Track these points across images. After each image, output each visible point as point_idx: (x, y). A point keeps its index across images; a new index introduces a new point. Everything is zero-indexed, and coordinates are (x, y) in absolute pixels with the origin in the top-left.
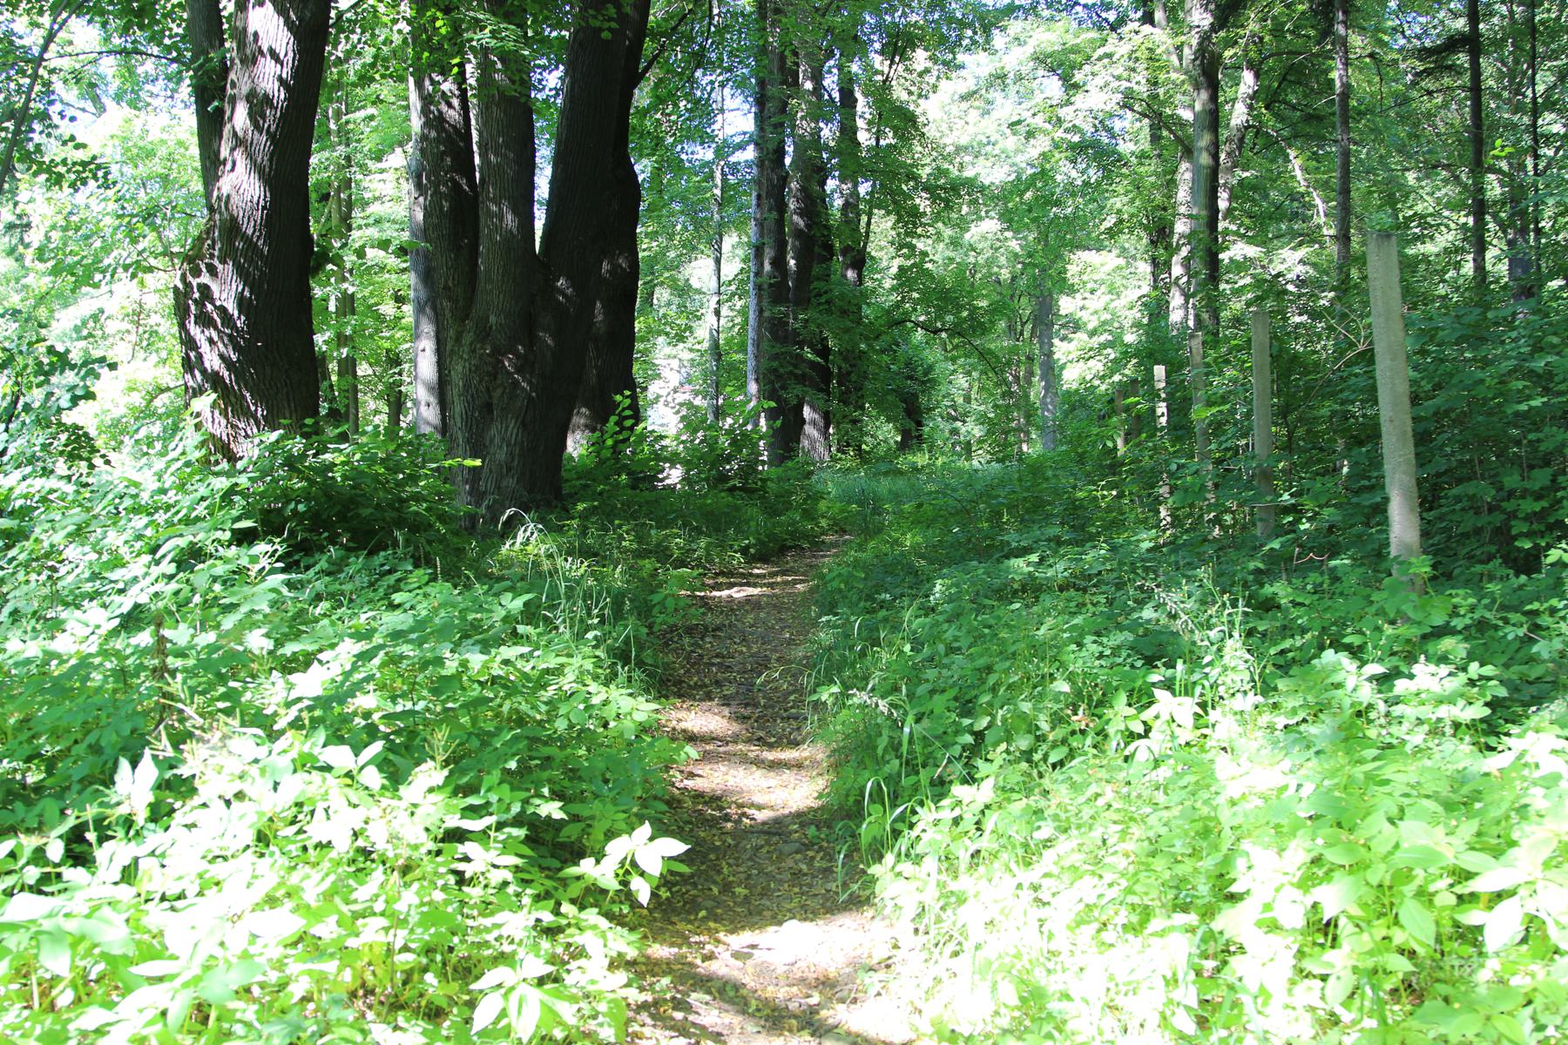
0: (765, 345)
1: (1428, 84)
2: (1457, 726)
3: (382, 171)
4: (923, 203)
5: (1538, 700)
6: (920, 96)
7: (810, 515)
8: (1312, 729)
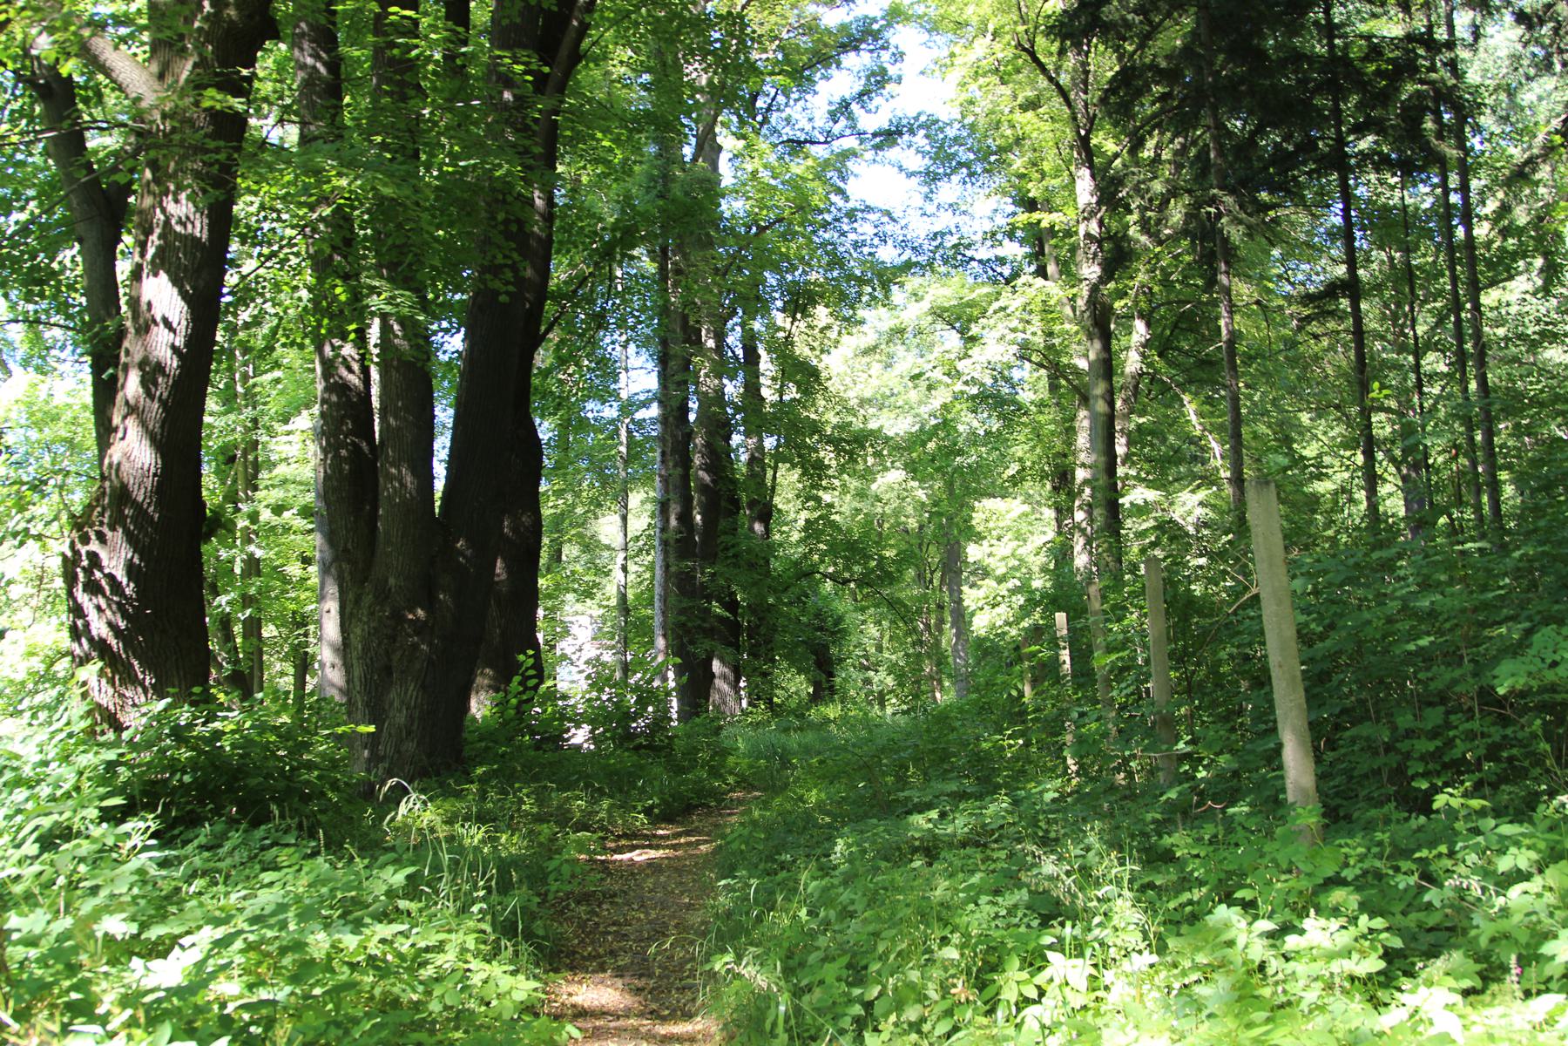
0: (672, 600)
1: (1314, 327)
2: (1352, 979)
3: (289, 433)
4: (827, 455)
5: (1432, 953)
6: (822, 351)
7: (715, 772)
8: (1202, 990)
